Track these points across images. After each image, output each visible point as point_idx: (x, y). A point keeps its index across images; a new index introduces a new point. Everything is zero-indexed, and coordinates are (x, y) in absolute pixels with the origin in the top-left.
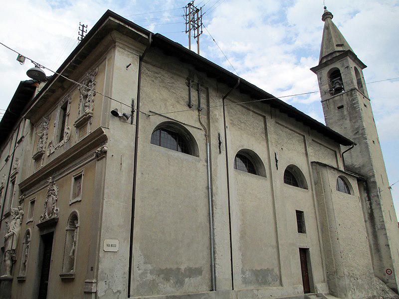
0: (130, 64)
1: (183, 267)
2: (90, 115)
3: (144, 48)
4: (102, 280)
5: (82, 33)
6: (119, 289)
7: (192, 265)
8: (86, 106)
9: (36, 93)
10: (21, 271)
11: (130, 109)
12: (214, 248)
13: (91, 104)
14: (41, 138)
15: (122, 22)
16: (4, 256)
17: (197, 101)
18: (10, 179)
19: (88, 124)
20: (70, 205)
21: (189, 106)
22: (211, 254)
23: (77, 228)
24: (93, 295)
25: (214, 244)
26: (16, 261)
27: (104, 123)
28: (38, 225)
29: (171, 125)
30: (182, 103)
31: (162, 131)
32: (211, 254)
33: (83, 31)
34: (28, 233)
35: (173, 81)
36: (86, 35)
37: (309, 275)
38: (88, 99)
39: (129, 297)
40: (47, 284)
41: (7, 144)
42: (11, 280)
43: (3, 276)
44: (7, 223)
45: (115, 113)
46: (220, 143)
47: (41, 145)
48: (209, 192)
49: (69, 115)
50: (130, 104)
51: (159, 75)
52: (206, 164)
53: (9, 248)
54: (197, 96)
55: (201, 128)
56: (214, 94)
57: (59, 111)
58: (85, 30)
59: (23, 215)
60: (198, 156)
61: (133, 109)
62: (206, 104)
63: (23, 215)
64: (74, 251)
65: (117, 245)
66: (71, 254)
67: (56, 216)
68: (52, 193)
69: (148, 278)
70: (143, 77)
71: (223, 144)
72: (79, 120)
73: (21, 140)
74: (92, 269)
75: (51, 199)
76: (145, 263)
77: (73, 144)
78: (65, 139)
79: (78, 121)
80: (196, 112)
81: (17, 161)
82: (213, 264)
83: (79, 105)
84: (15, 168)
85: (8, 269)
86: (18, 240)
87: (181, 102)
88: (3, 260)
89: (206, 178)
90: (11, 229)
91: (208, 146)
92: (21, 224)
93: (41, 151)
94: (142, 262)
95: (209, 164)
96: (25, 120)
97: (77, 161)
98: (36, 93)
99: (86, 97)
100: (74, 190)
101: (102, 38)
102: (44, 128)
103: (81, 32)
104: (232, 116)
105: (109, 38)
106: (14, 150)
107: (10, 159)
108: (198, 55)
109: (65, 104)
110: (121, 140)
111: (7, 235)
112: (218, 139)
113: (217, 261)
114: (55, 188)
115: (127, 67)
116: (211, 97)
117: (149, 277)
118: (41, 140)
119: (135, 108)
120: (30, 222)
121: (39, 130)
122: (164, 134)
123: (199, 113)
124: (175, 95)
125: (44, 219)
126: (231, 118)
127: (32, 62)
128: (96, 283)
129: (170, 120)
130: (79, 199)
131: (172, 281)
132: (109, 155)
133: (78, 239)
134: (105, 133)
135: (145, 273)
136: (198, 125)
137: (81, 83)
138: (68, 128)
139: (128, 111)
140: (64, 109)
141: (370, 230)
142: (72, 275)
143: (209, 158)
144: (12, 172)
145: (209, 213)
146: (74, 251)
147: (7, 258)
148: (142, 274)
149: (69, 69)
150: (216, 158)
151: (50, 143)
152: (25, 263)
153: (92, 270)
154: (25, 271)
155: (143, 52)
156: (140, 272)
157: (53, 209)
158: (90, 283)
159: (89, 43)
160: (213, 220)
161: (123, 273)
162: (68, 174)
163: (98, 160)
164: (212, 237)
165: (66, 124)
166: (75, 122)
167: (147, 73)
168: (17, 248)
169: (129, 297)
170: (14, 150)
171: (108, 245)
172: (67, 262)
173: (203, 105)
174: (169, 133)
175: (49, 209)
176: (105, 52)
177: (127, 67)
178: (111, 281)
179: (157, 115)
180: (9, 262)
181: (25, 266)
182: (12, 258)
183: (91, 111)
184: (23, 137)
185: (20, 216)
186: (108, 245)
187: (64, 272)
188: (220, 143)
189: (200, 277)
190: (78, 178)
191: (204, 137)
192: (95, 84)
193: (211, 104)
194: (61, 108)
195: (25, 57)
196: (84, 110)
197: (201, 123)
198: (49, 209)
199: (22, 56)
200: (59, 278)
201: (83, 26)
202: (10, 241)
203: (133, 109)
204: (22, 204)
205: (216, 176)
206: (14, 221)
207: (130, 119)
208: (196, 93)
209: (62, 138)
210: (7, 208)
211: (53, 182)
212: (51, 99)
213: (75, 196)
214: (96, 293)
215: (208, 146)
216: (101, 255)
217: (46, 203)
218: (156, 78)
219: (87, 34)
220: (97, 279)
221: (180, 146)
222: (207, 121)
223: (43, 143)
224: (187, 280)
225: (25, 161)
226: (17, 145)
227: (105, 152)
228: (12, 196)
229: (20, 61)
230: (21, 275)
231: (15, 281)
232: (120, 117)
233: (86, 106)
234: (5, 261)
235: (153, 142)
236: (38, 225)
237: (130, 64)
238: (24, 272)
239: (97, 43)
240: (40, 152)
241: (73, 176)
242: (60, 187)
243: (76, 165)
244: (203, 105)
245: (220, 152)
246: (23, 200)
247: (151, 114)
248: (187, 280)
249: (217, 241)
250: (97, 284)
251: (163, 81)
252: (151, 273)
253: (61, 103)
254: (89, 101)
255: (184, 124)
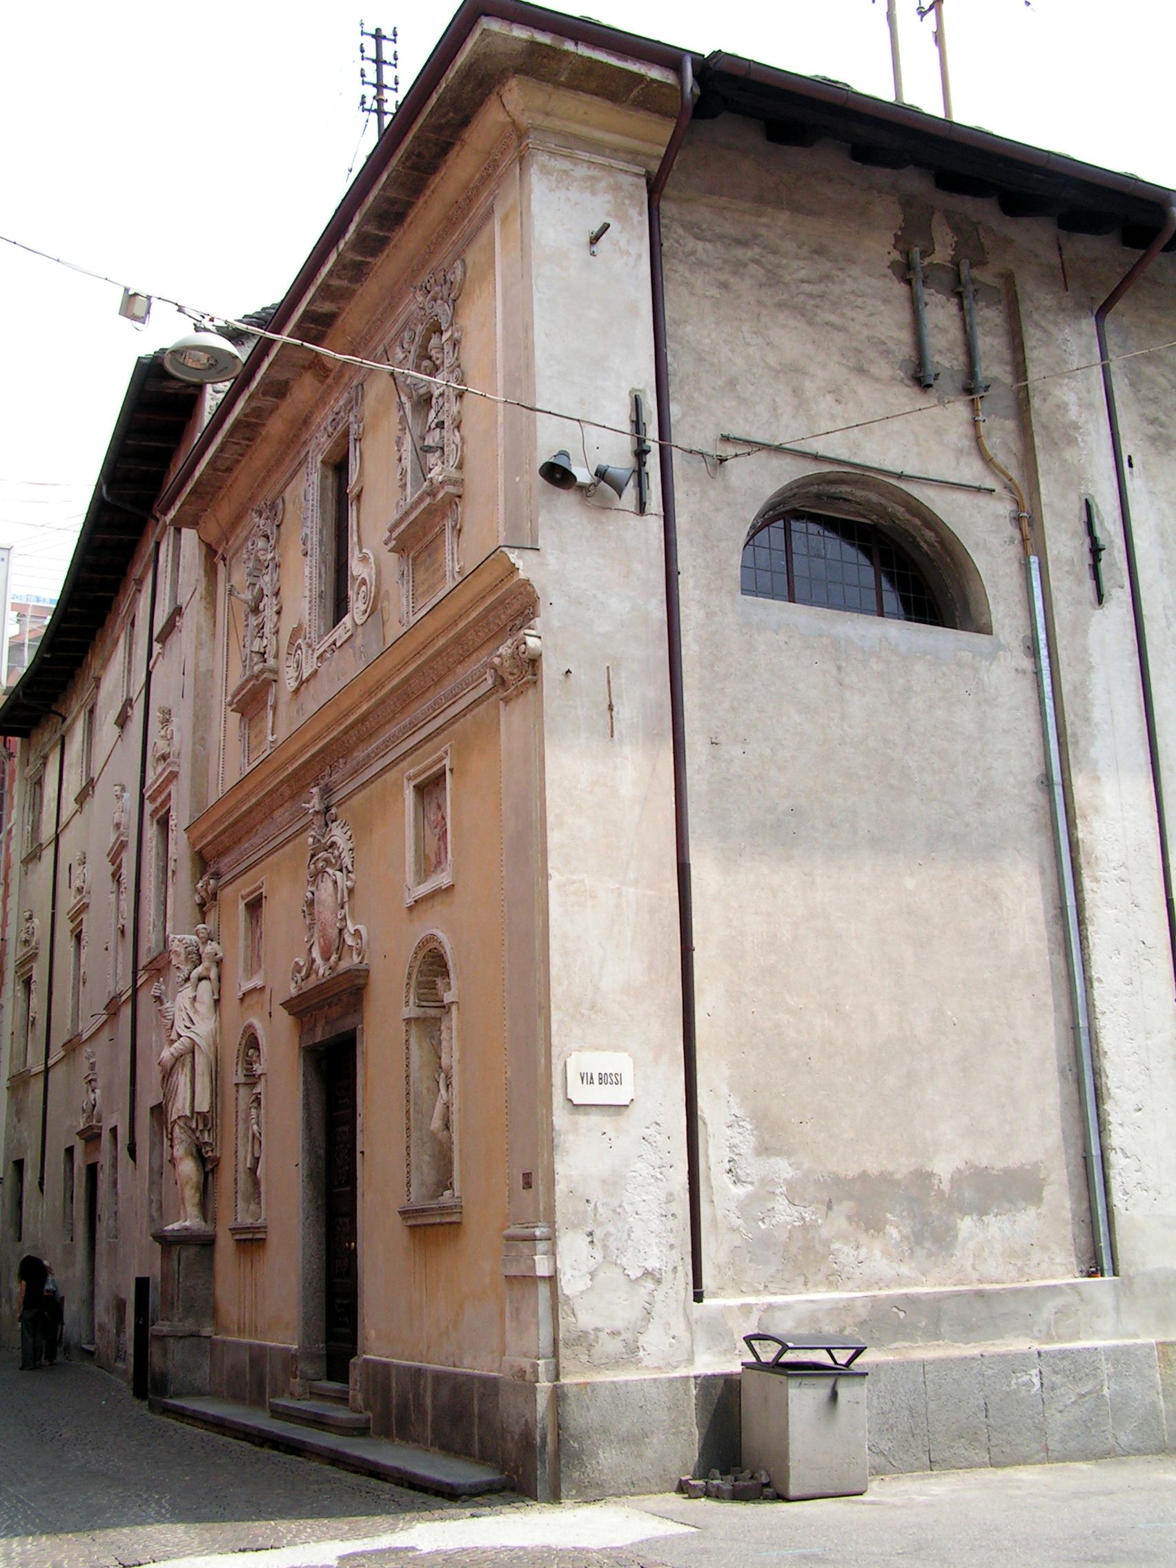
0: (606, 227)
1: (944, 1167)
2: (450, 489)
3: (664, 131)
4: (574, 1226)
5: (379, 72)
6: (652, 1264)
7: (986, 1156)
8: (428, 450)
9: (206, 416)
10: (241, 1203)
11: (627, 444)
12: (1097, 1073)
13: (451, 437)
14: (256, 610)
15: (543, 29)
16: (166, 1143)
17: (960, 351)
18: (149, 807)
19: (448, 532)
20: (411, 909)
21: (921, 379)
22: (1082, 1102)
23: (446, 1008)
24: (544, 1290)
25: (1096, 1052)
26: (217, 1161)
27: (514, 526)
28: (287, 1005)
29: (834, 489)
30: (882, 369)
31: (795, 525)
32: (1082, 1102)
33: (380, 86)
34: (252, 1042)
35: (825, 266)
36: (399, 108)
37: (322, 1230)
38: (432, 414)
39: (698, 1297)
40: (353, 1254)
41: (116, 643)
42: (207, 1243)
43: (176, 1226)
44: (158, 999)
45: (557, 474)
46: (1096, 550)
47: (257, 645)
48: (1052, 801)
49: (359, 496)
50: (621, 417)
51: (754, 252)
52: (1027, 664)
53: (180, 1106)
54: (957, 323)
55: (989, 483)
56: (1047, 300)
57: (315, 478)
58: (388, 80)
59: (219, 963)
60: (986, 629)
61: (641, 442)
62: (1007, 355)
63: (219, 963)
64: (447, 1107)
65: (628, 1077)
66: (436, 1124)
67: (356, 959)
68: (326, 860)
69: (780, 1218)
70: (675, 272)
71: (1114, 555)
72: (407, 514)
73: (171, 626)
74: (528, 1181)
75: (326, 887)
76: (764, 1150)
77: (394, 631)
78: (357, 606)
79: (401, 520)
80: (959, 410)
81: (166, 722)
82: (1095, 1151)
83: (399, 443)
84: (164, 757)
85: (191, 1196)
86: (216, 1076)
87: (874, 369)
88: (166, 1157)
89: (1038, 741)
90: (179, 1027)
91: (1035, 574)
92: (217, 1002)
93: (262, 671)
94: (745, 1149)
95: (1045, 663)
96: (178, 531)
97: (420, 708)
98: (206, 416)
99: (424, 402)
100: (419, 840)
101: (465, 122)
102: (260, 568)
103: (371, 69)
104: (1155, 401)
105: (491, 119)
106: (149, 674)
107: (137, 713)
108: (948, 124)
109: (337, 444)
110: (601, 596)
111: (167, 1053)
112: (1082, 528)
113: (1118, 1136)
114: (338, 834)
115: (595, 239)
116: (1030, 315)
117: (784, 1213)
118: (253, 621)
119: (652, 432)
120: (254, 990)
121: (240, 576)
122: (807, 535)
123: (975, 411)
124: (839, 338)
125: (308, 976)
126: (1152, 410)
127: (180, 310)
128: (551, 1239)
129: (826, 468)
130: (442, 879)
131: (894, 1233)
132: (550, 670)
133: (456, 1055)
134: (522, 575)
135: (766, 1188)
136: (972, 471)
137: (386, 356)
138: (364, 559)
139: (618, 455)
140: (339, 467)
141: (1076, 1113)
142: (444, 1210)
143: (1042, 636)
144: (151, 776)
145: (1063, 909)
146: (447, 1107)
147: (179, 1151)
148: (751, 1199)
149: (335, 282)
150: (1080, 628)
151: (296, 633)
152: (253, 1170)
153: (528, 1184)
154: (259, 1203)
155: (662, 150)
156: (740, 1191)
157: (341, 931)
158: (524, 1239)
159: (409, 154)
160: (1083, 938)
161: (663, 1197)
162: (384, 770)
163: (507, 700)
164: (1082, 1023)
165: (353, 539)
166: (391, 531)
167: (693, 253)
168: (214, 1104)
169: (698, 1297)
170: (149, 674)
171: (586, 1078)
172: (424, 1159)
173: (993, 368)
174: (830, 524)
175: (323, 930)
176: (484, 181)
177: (595, 239)
178: (611, 1229)
179: (763, 455)
180: (188, 1168)
181: (256, 1183)
182: (199, 1151)
183: (454, 474)
184: (178, 611)
185: (208, 969)
186: (586, 1078)
187: (417, 1197)
188: (1096, 550)
189: (1032, 1211)
190: (430, 787)
191: (1010, 530)
192: (456, 344)
193: (1036, 354)
194: (323, 462)
195: (149, 298)
196: (424, 470)
197: (988, 461)
198: (323, 930)
199: (136, 294)
200: (397, 1226)
201: (378, 36)
202: (182, 1080)
203: (641, 442)
204: (212, 917)
205: (1087, 720)
206: (188, 992)
207: (630, 492)
208: (952, 306)
209: (340, 607)
210: (153, 937)
211: (328, 809)
212: (276, 427)
213: (428, 864)
214: (552, 1279)
215: (1035, 574)
216: (560, 1117)
217: (311, 904)
218: (738, 267)
219: (400, 96)
220: (552, 1224)
221: (891, 581)
222: (1016, 445)
223: (266, 630)
224: (966, 1225)
225: (201, 720)
226: (157, 647)
227: (534, 662)
228: (165, 882)
229: (135, 318)
230: (245, 1219)
231: (225, 1244)
232: (583, 488)
233: (428, 450)
234: (172, 1161)
235: (753, 585)
236: (287, 1005)
237: (606, 227)
238: (253, 1207)
239: (444, 149)
240: (257, 677)
241: (409, 779)
242: (361, 829)
243: (414, 728)
244: (993, 368)
245: (1100, 598)
246: (214, 896)
247: (730, 450)
248: (966, 1225)
249: (1108, 1040)
250: (554, 1245)
251: (773, 279)
252: (794, 1194)
253: (319, 445)
254: (440, 425)
255: (900, 476)
